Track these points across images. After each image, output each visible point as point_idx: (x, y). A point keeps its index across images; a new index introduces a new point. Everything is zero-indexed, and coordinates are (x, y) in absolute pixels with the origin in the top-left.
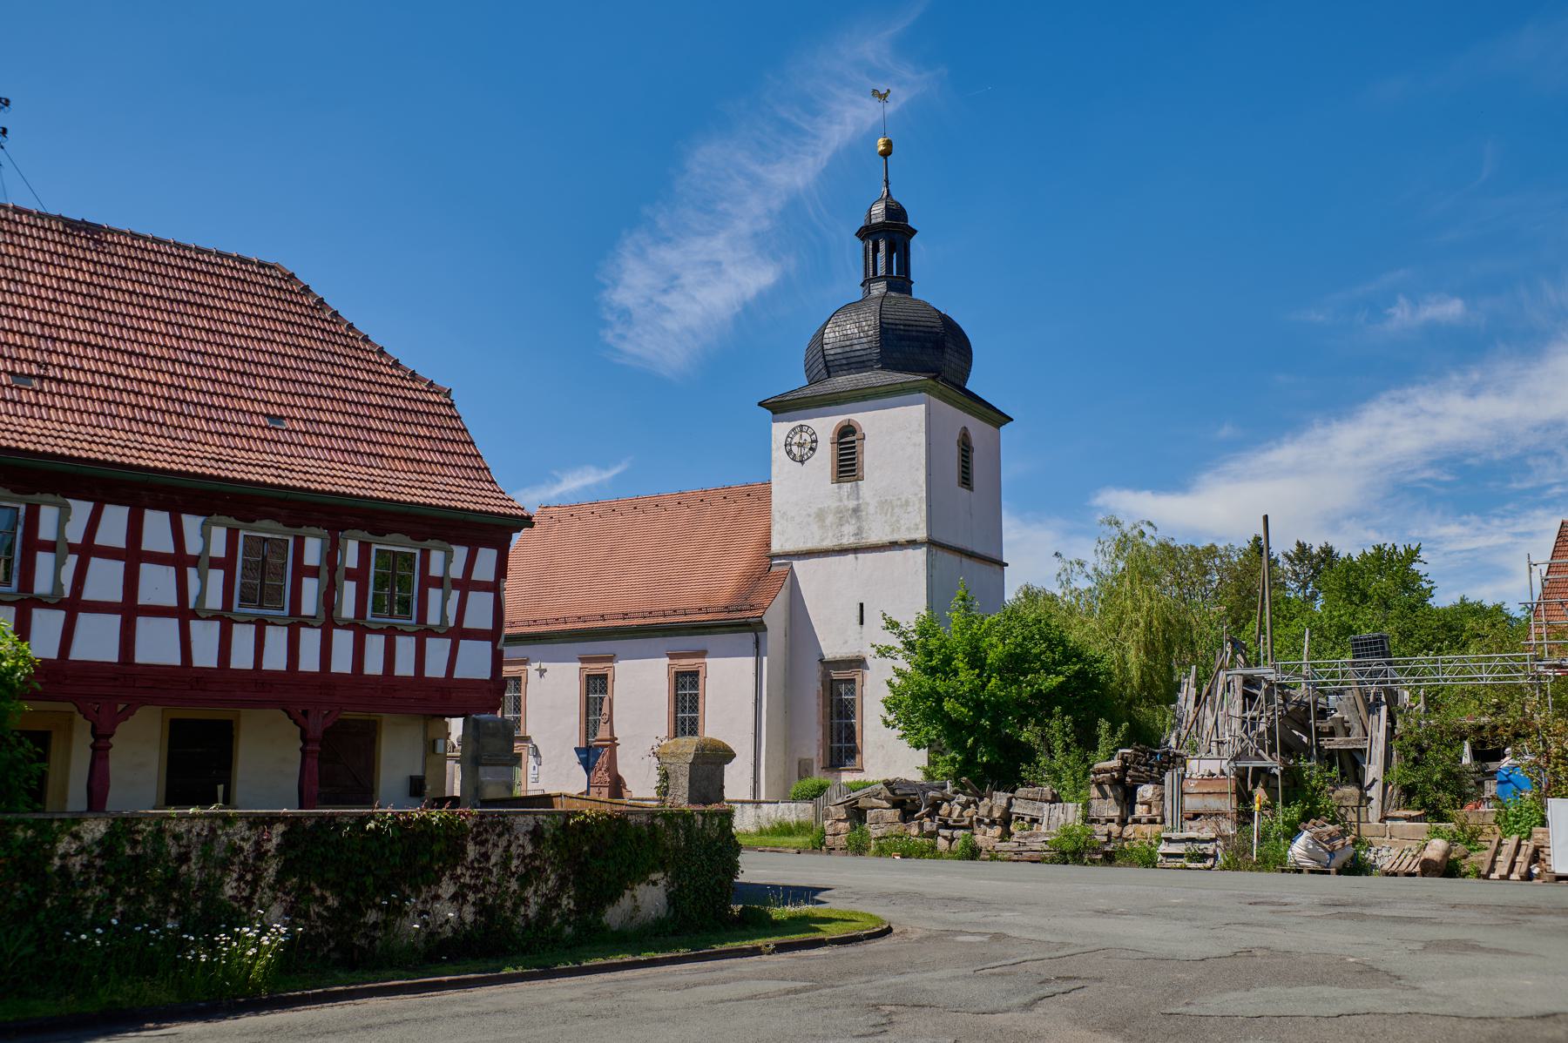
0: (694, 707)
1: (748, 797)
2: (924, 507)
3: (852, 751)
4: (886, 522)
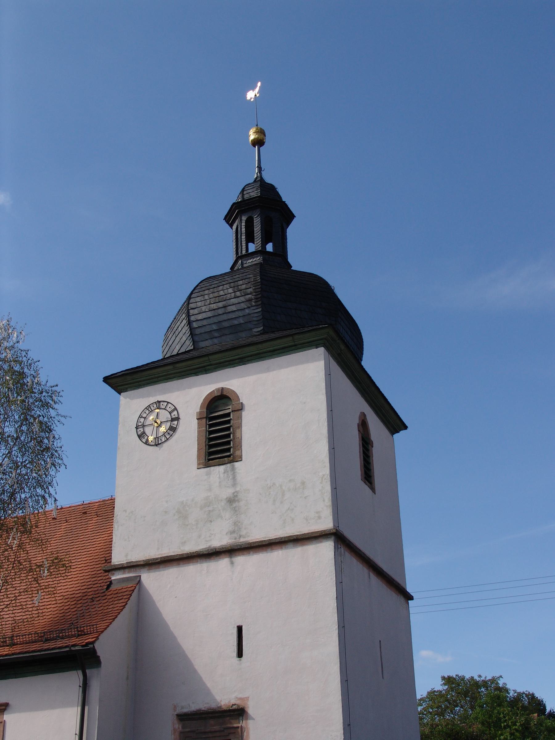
2: (328, 488)
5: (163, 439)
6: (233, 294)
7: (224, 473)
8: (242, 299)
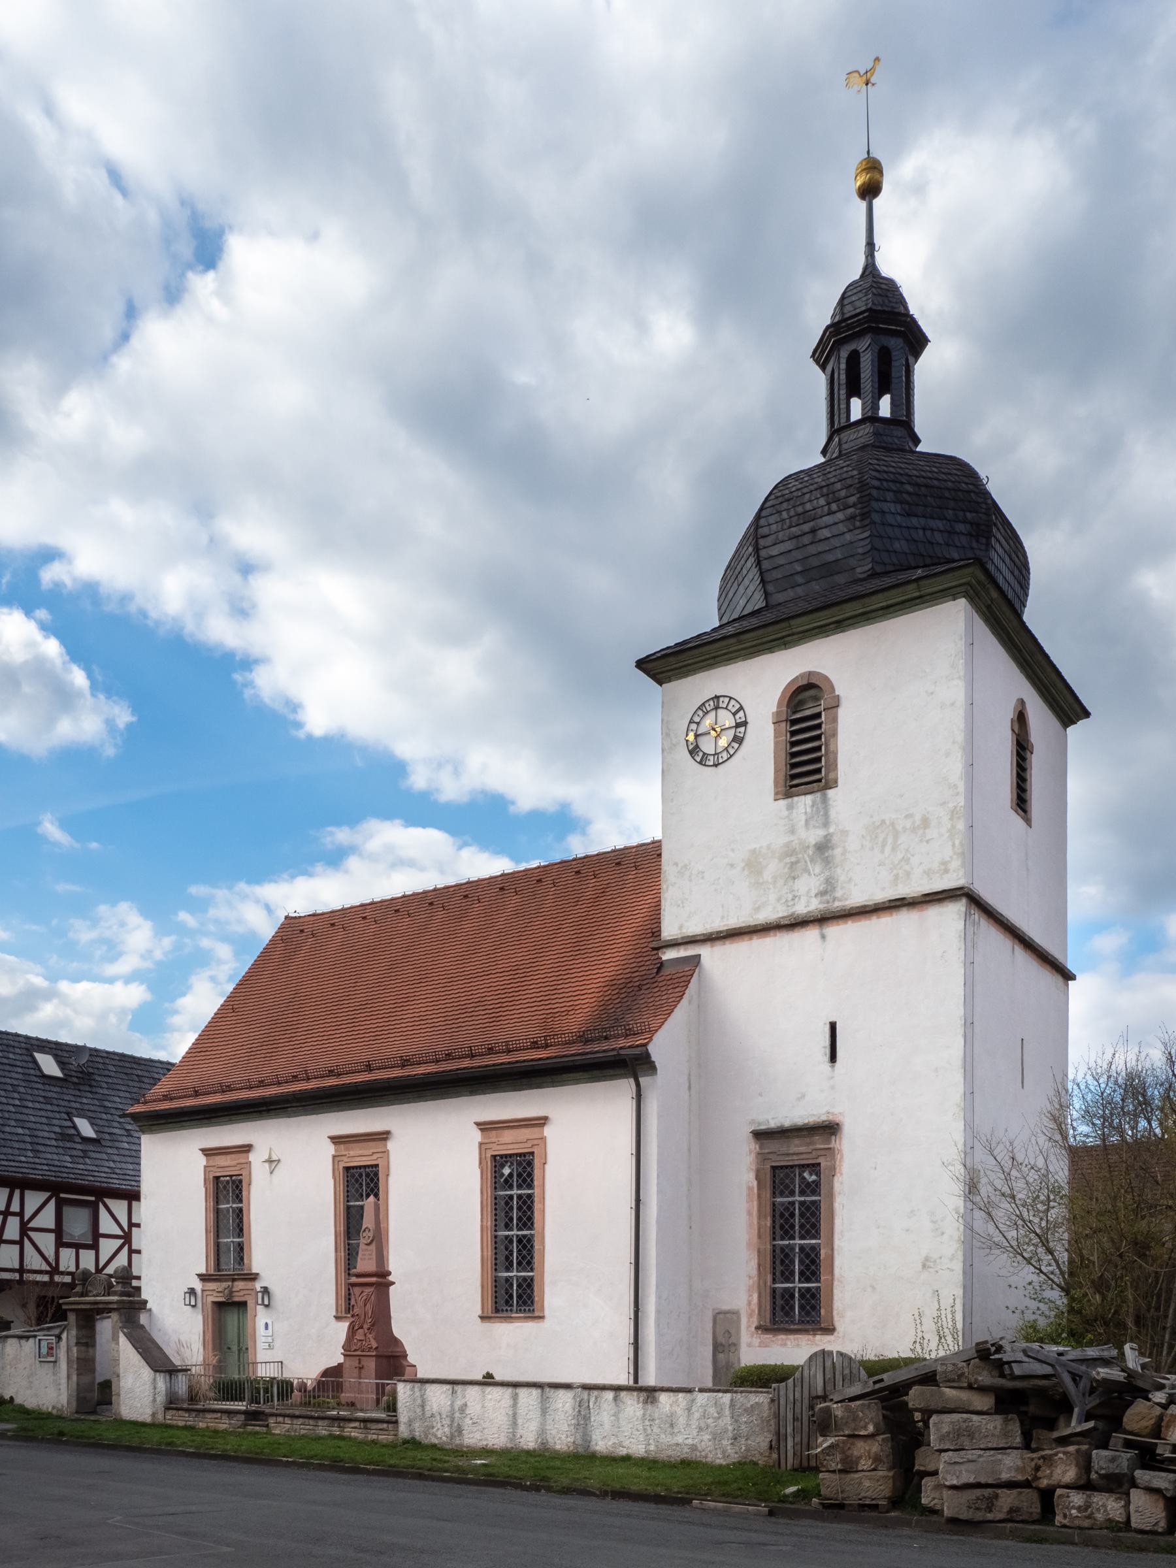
0: (527, 1220)
1: (622, 1377)
3: (813, 1296)
4: (881, 864)
5: (725, 755)
6: (826, 508)
7: (813, 806)
8: (840, 516)
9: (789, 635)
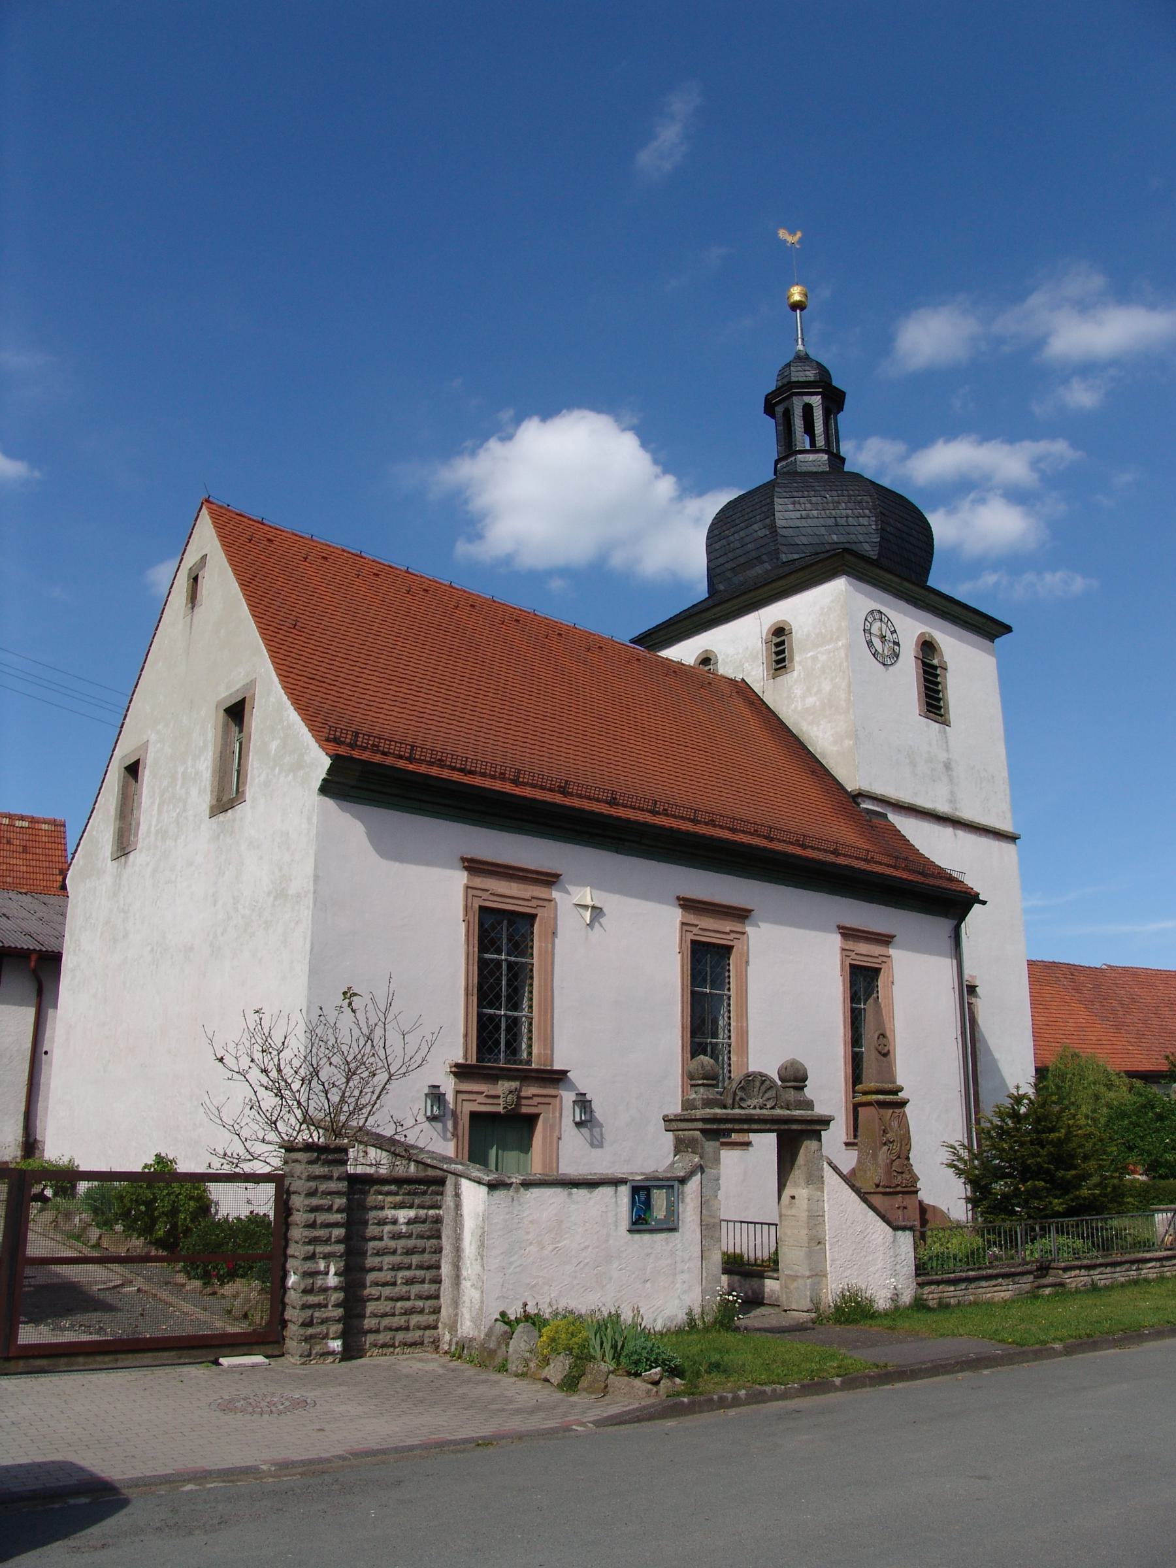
9: (920, 600)
